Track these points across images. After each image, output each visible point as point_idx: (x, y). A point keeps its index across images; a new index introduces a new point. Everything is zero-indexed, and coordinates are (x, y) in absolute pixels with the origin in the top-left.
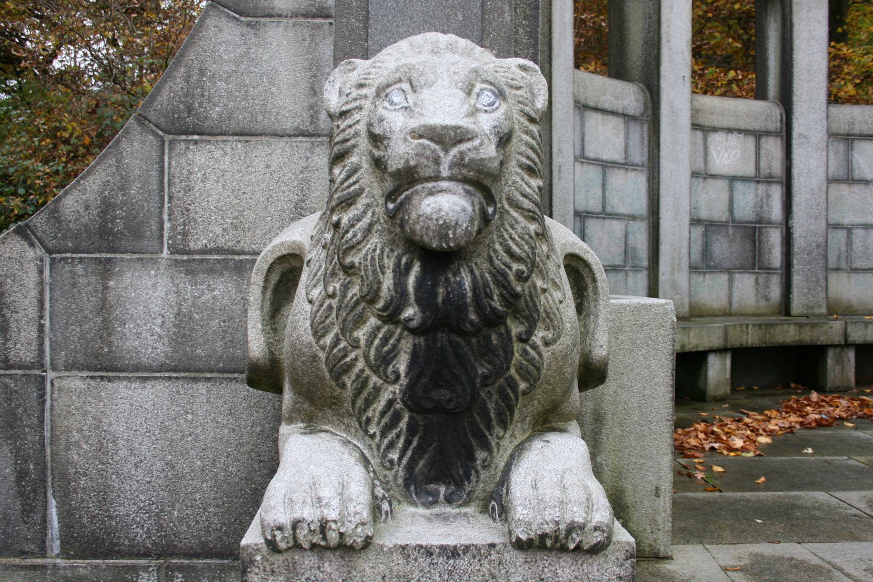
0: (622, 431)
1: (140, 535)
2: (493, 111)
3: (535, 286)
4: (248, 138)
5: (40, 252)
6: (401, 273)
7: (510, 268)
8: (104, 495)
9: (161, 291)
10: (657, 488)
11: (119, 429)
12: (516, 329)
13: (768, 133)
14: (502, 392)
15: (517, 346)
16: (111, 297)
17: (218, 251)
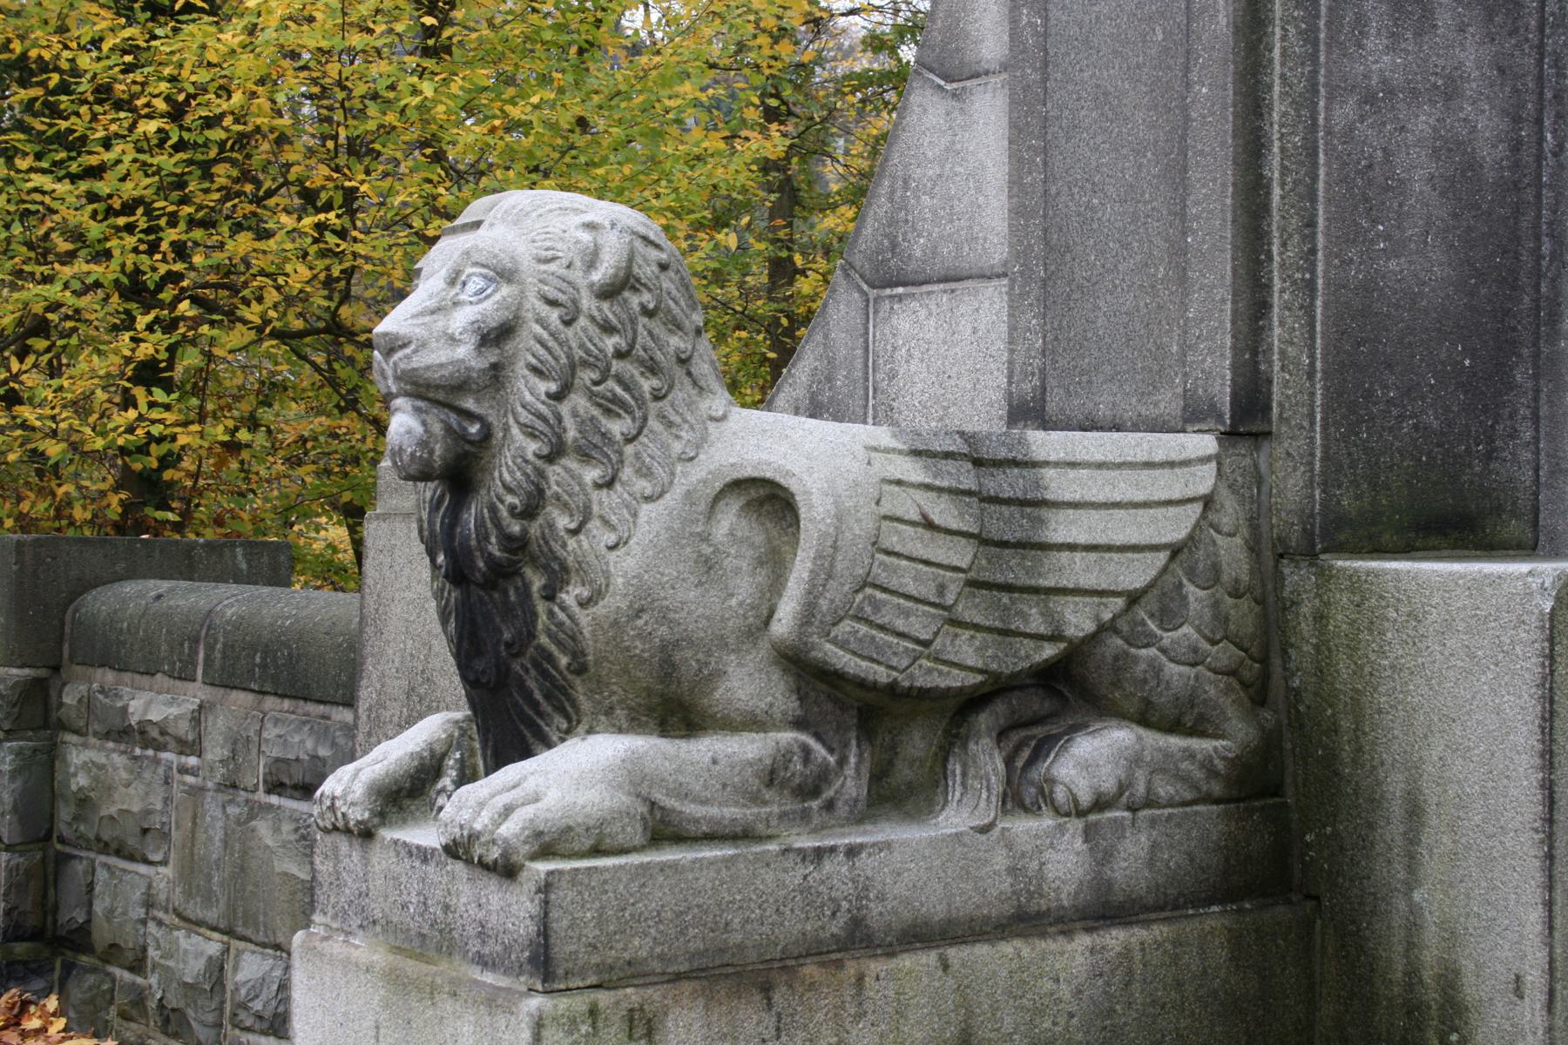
0: (1454, 842)
2: (480, 301)
3: (552, 526)
4: (953, 285)
7: (502, 502)
10: (1518, 978)
12: (537, 582)
14: (537, 665)
15: (541, 607)
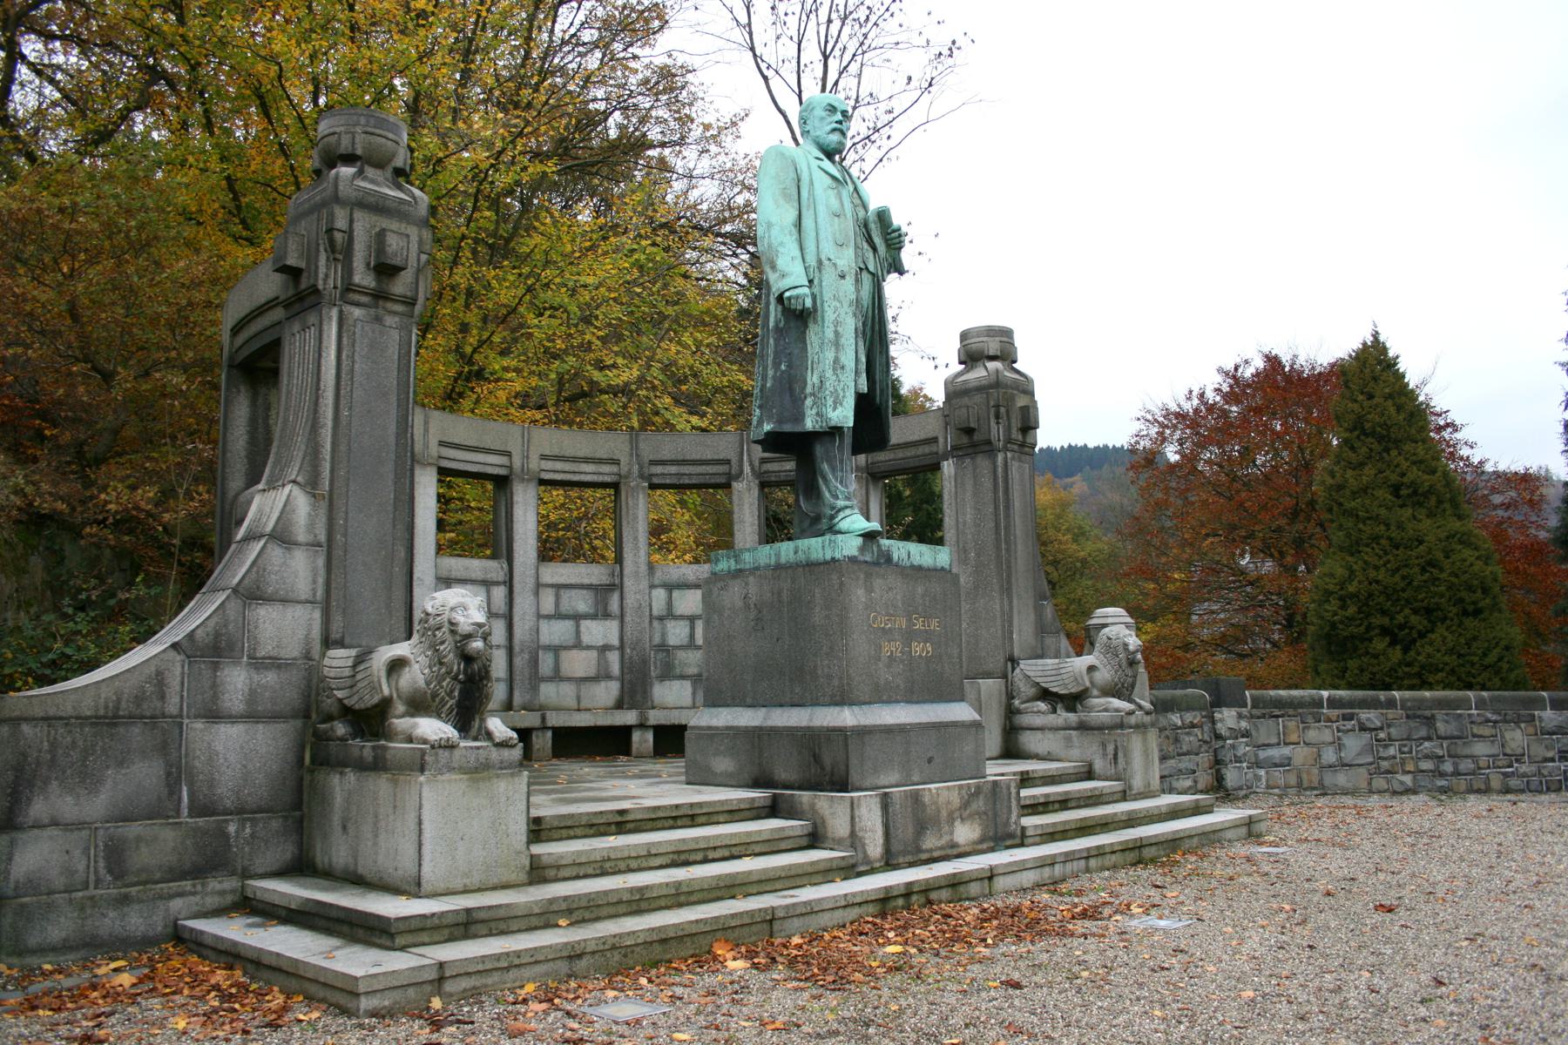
1: (228, 803)
5: (183, 657)
6: (459, 665)
8: (212, 784)
9: (242, 678)
11: (220, 748)
13: (497, 583)
16: (218, 680)
17: (270, 658)
